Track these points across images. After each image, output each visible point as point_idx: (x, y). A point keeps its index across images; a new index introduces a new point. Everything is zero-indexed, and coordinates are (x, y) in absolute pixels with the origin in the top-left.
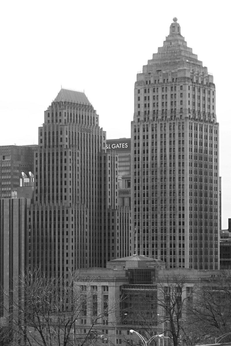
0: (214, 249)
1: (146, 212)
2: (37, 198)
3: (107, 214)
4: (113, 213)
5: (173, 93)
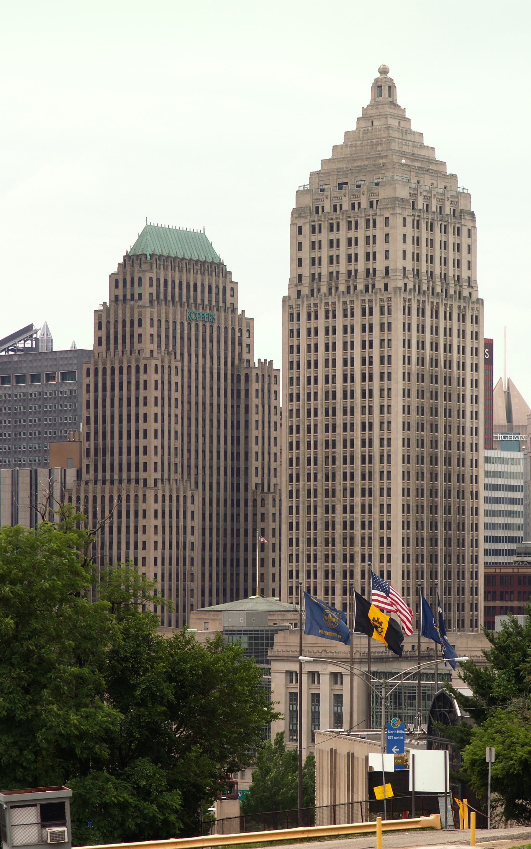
0: (468, 583)
1: (312, 499)
2: (88, 466)
3: (250, 503)
4: (263, 500)
5: (370, 233)
